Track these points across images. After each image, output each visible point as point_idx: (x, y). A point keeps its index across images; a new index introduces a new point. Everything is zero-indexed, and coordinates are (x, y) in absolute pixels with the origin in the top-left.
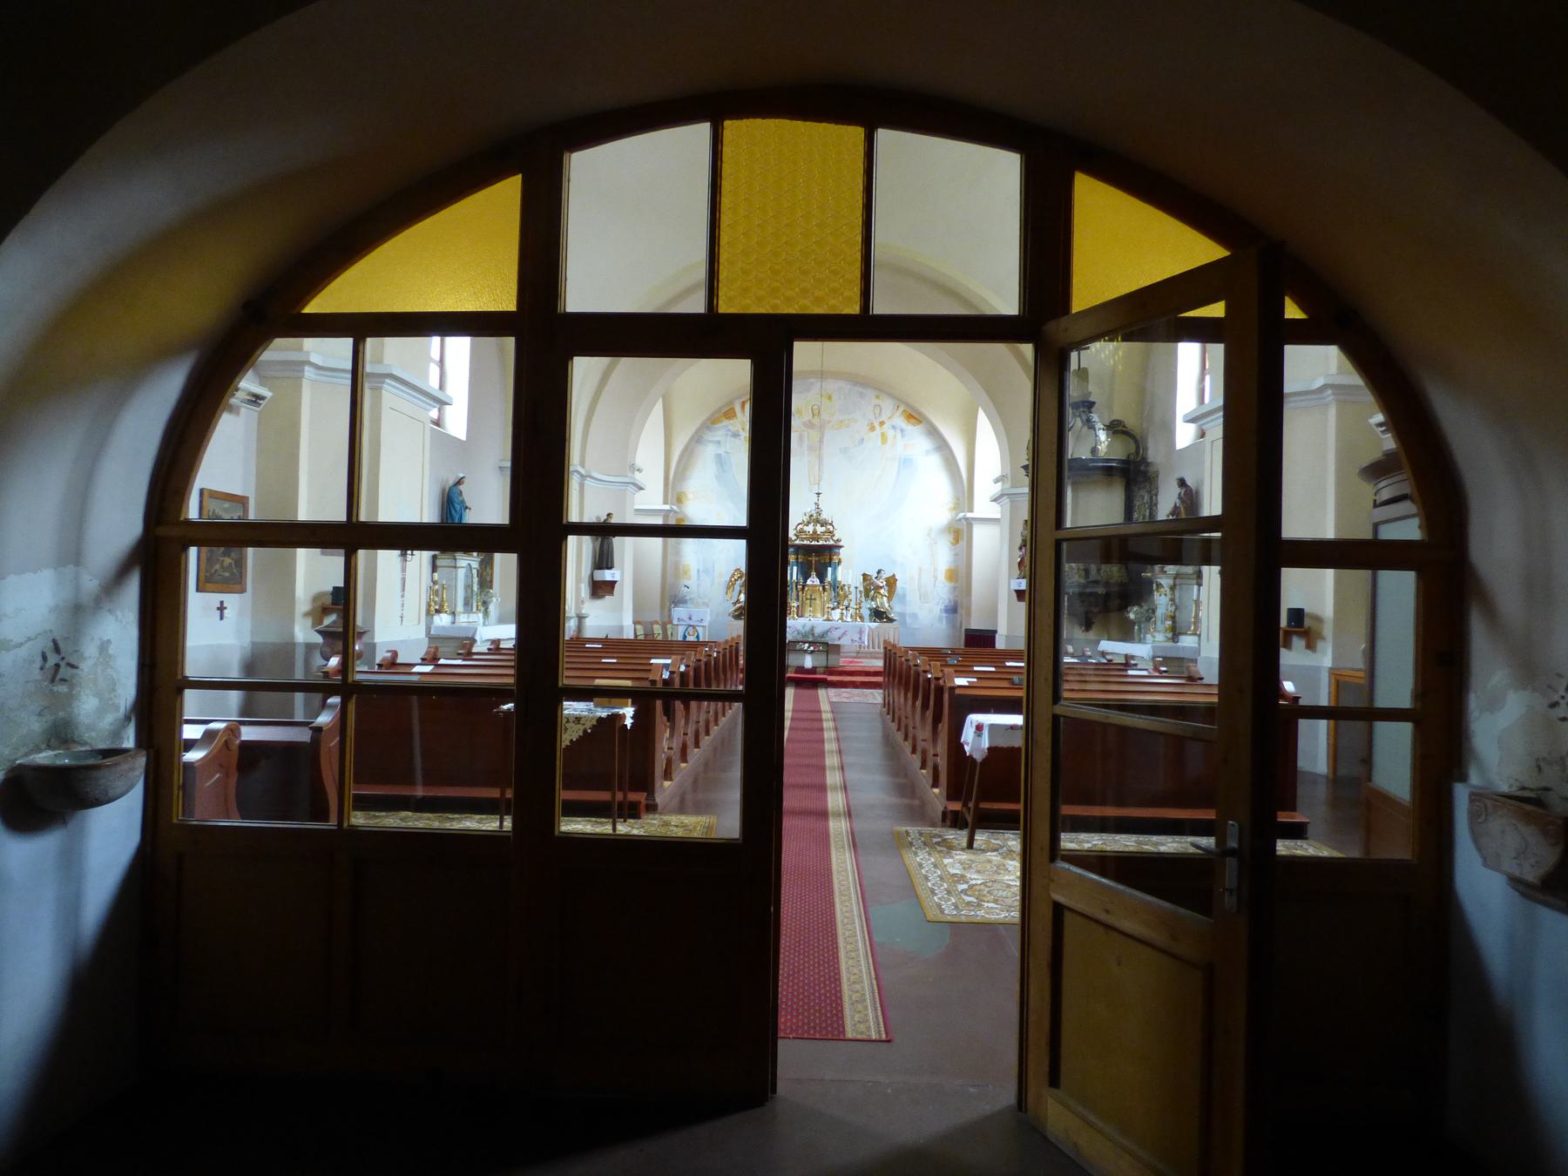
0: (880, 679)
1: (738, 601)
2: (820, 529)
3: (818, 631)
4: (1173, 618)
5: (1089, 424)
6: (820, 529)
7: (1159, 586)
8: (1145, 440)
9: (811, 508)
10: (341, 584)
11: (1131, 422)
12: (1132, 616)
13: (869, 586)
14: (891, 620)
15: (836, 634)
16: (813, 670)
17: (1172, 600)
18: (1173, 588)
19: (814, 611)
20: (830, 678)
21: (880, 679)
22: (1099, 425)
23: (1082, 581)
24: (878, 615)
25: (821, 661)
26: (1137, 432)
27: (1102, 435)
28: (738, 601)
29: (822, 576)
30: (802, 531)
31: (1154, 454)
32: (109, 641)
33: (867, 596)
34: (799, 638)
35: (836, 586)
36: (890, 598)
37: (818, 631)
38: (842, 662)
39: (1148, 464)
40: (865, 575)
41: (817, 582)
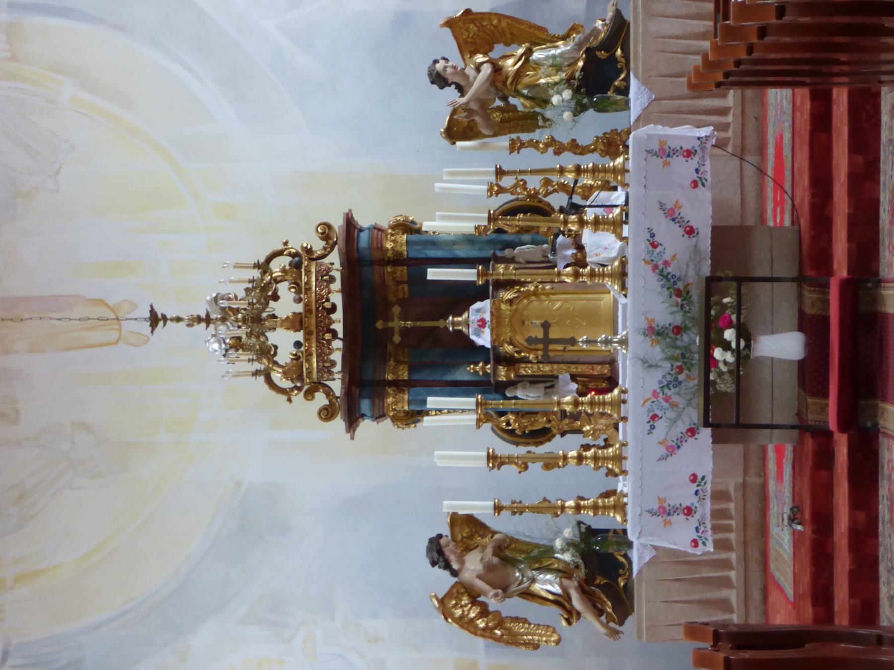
0: (841, 98)
1: (562, 602)
2: (286, 304)
3: (664, 313)
6: (286, 304)
9: (210, 343)
13: (491, 113)
14: (619, 29)
15: (673, 242)
16: (812, 327)
19: (592, 318)
20: (841, 268)
21: (841, 98)
24: (599, 76)
25: (780, 300)
28: (562, 602)
29: (462, 297)
30: (295, 371)
33: (529, 121)
34: (692, 381)
35: (490, 247)
36: (538, 36)
37: (664, 313)
38: (780, 215)
40: (457, 131)
41: (482, 309)
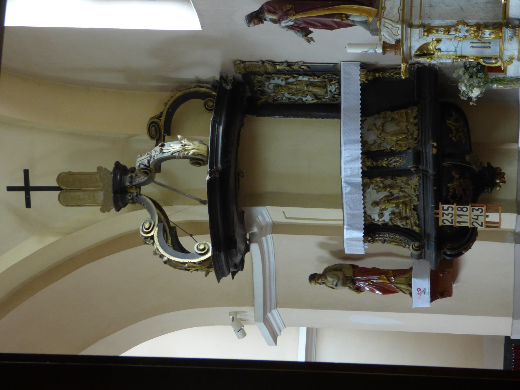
4: (479, 27)
5: (153, 169)
7: (424, 52)
8: (182, 84)
10: (189, 160)
11: (151, 108)
12: (475, 93)
17: (447, 30)
18: (428, 29)
22: (156, 153)
23: (415, 180)
26: (166, 96)
27: (173, 147)
31: (207, 69)
32: (117, 164)
39: (223, 78)
